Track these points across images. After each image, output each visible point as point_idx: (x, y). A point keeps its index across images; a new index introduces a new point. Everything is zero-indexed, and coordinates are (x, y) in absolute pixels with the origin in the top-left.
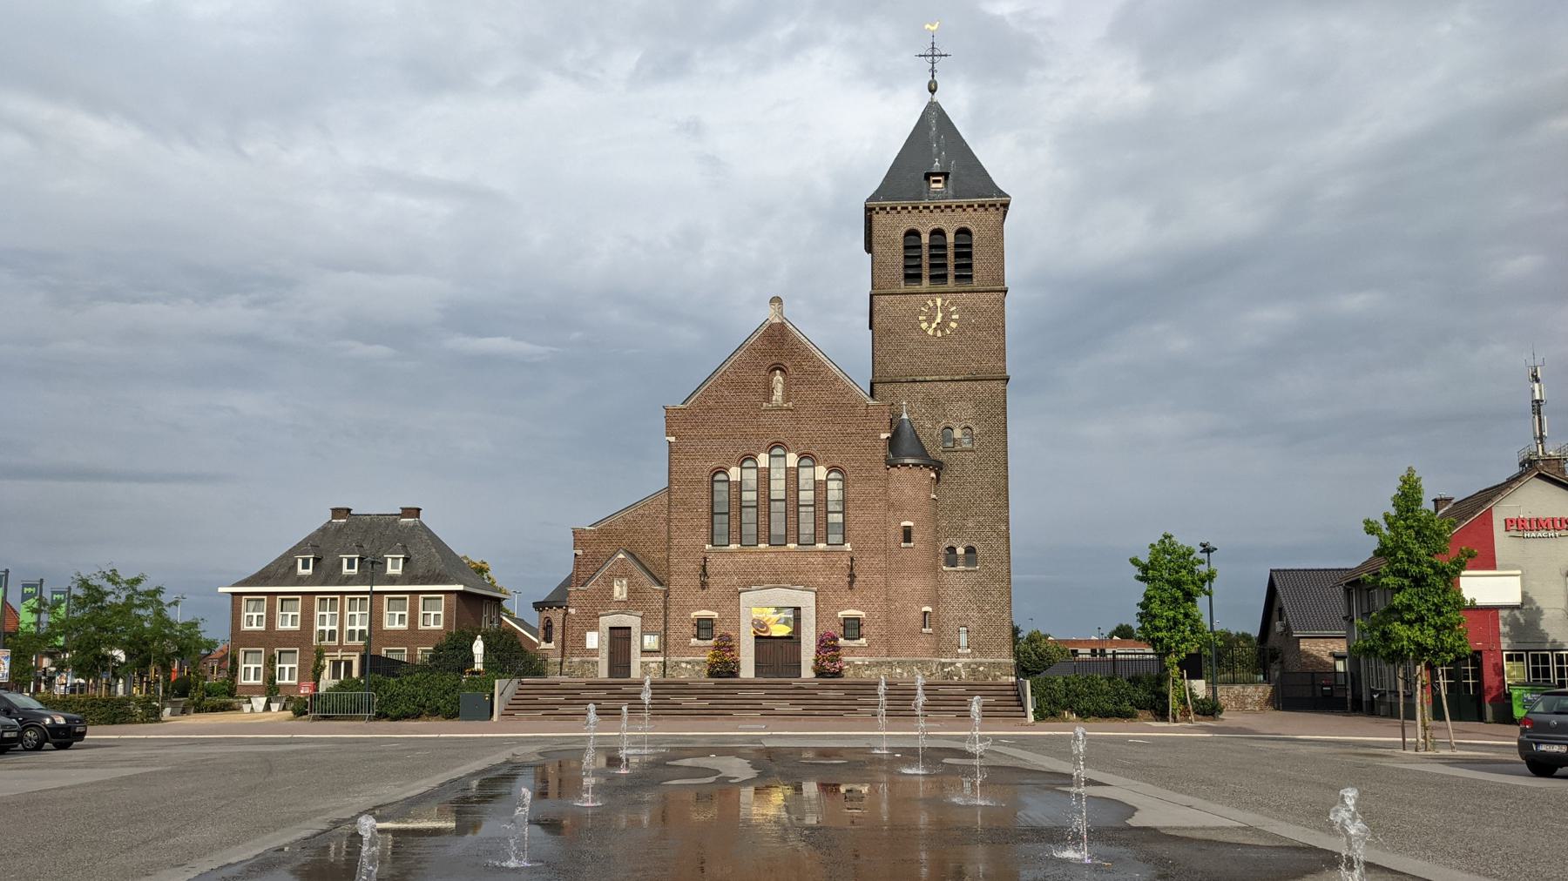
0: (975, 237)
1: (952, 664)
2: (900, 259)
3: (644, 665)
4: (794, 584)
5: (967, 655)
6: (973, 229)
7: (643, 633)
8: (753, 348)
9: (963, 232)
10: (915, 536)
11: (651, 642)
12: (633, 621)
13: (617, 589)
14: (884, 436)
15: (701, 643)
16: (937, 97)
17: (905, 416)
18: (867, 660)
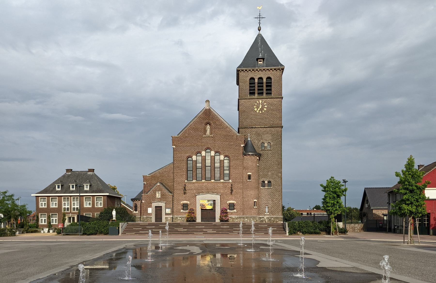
0: (273, 80)
1: (263, 218)
3: (166, 218)
5: (268, 215)
6: (272, 77)
7: (166, 208)
10: (252, 177)
12: (162, 204)
13: (157, 195)
14: (242, 145)
15: (184, 211)
16: (261, 32)
17: (249, 139)
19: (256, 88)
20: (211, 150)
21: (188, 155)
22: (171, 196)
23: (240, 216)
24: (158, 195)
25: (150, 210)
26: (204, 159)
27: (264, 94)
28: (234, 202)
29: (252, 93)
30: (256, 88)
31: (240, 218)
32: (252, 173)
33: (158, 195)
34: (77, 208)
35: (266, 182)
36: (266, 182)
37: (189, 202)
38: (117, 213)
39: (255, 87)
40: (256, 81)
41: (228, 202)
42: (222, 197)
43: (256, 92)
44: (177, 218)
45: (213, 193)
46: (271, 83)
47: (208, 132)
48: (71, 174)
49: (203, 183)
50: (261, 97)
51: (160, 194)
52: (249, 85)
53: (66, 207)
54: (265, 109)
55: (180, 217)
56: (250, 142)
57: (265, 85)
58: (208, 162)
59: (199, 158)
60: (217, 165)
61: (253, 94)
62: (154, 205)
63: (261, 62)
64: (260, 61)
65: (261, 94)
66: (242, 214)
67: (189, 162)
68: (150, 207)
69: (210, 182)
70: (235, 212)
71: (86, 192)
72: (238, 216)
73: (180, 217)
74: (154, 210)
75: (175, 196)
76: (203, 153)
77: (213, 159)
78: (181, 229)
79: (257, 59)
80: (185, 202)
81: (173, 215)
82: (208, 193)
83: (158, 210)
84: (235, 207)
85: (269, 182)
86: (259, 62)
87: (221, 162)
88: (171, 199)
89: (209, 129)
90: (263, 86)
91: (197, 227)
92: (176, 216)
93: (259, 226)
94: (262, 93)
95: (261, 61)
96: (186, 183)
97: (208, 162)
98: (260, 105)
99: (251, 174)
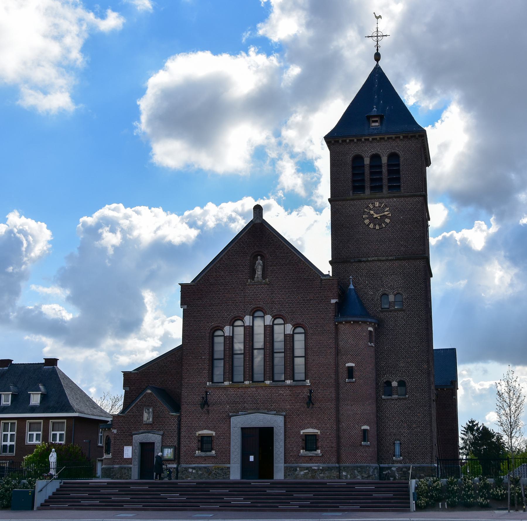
0: (402, 159)
1: (390, 468)
2: (350, 175)
5: (400, 462)
6: (401, 154)
7: (163, 447)
9: (393, 156)
10: (356, 374)
12: (155, 438)
13: (145, 415)
14: (333, 301)
15: (203, 454)
16: (380, 63)
17: (352, 287)
18: (322, 466)
19: (367, 177)
20: (265, 313)
21: (214, 324)
22: (176, 420)
23: (330, 465)
24: (147, 417)
25: (128, 452)
26: (249, 332)
27: (385, 190)
28: (316, 431)
29: (358, 187)
30: (367, 177)
31: (330, 469)
33: (147, 417)
34: (12, 446)
35: (394, 384)
36: (394, 384)
37: (214, 433)
38: (60, 461)
39: (363, 174)
40: (367, 161)
42: (288, 420)
43: (367, 184)
44: (186, 469)
45: (268, 410)
46: (398, 165)
47: (259, 273)
48: (8, 370)
49: (247, 387)
50: (378, 195)
51: (151, 415)
52: (350, 170)
53: (8, 443)
55: (193, 468)
56: (353, 293)
57: (385, 170)
58: (259, 340)
59: (240, 332)
60: (279, 345)
61: (362, 189)
62: (138, 438)
63: (377, 124)
64: (374, 122)
65: (377, 188)
66: (334, 459)
67: (216, 340)
68: (129, 443)
69: (262, 384)
70: (317, 456)
71: (33, 409)
72: (325, 465)
73: (193, 468)
74: (138, 451)
75: (184, 419)
76: (248, 320)
77: (269, 331)
78: (175, 496)
79: (369, 118)
80: (206, 432)
81: (179, 463)
82: (257, 410)
84: (319, 444)
85: (402, 384)
86: (373, 124)
87: (289, 339)
88: (175, 427)
89: (260, 267)
90: (381, 173)
92: (184, 466)
94: (380, 188)
95: (376, 121)
96: (209, 387)
97: (259, 340)
98: (378, 210)
99: (353, 365)
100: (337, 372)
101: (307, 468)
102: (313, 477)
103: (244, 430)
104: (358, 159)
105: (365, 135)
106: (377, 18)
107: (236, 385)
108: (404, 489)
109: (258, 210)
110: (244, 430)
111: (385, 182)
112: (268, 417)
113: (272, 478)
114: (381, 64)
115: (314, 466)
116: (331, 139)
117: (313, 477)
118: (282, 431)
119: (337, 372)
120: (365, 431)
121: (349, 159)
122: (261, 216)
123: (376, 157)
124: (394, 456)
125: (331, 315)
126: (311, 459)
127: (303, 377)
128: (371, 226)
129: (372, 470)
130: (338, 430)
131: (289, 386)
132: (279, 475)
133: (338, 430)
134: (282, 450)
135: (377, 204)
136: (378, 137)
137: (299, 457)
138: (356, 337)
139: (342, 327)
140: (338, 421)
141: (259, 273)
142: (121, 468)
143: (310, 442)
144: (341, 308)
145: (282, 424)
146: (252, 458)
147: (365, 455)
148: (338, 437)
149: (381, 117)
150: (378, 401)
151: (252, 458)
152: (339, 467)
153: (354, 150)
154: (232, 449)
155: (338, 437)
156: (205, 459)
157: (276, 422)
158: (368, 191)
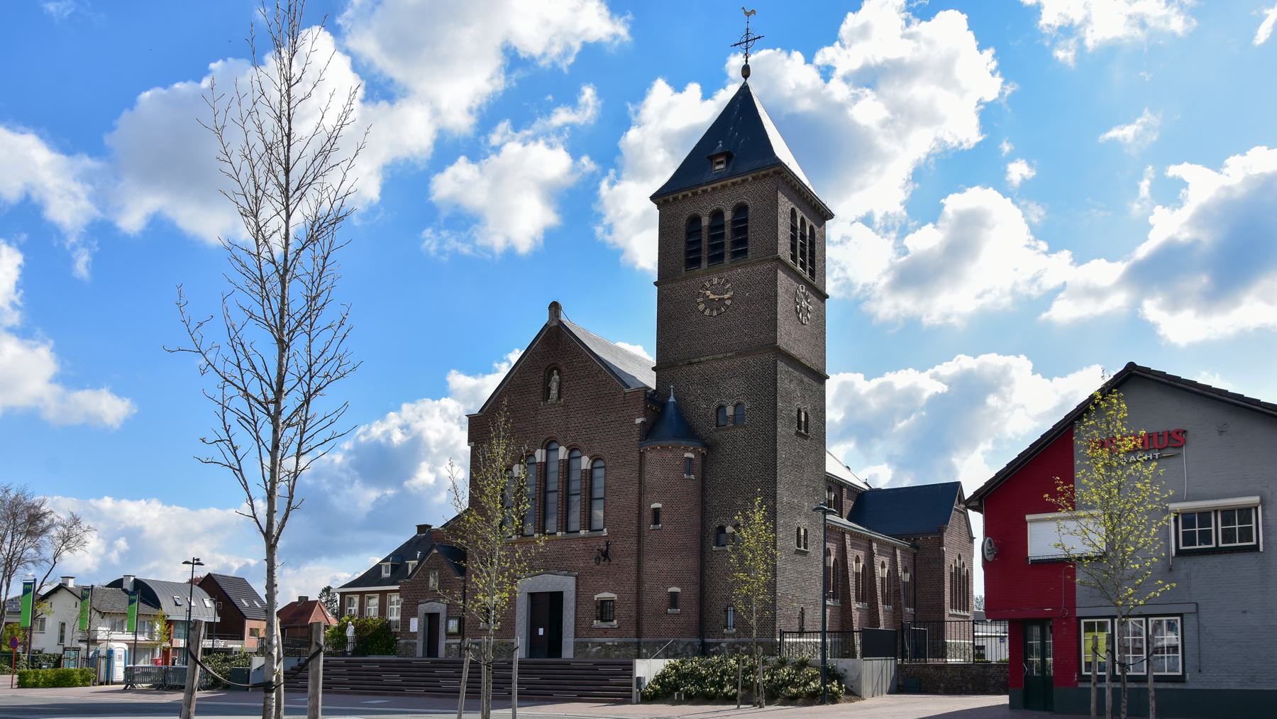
0: (750, 211)
1: (718, 644)
2: (682, 246)
3: (448, 646)
4: (560, 570)
5: (732, 636)
6: (750, 203)
7: (448, 618)
8: (91, 388)
9: (741, 209)
10: (663, 517)
11: (453, 625)
12: (439, 607)
13: (432, 580)
14: (638, 421)
15: (605, 625)
16: (749, 81)
17: (672, 399)
18: (617, 641)
24: (433, 582)
31: (626, 645)
32: (665, 503)
39: (700, 241)
41: (596, 597)
47: (554, 392)
54: (701, 307)
62: (424, 608)
63: (722, 166)
64: (718, 163)
66: (633, 633)
83: (432, 619)
91: (613, 681)
93: (601, 669)
100: (640, 515)
101: (600, 644)
102: (607, 656)
103: (532, 596)
104: (695, 220)
105: (701, 185)
106: (748, 14)
107: (525, 539)
108: (333, 679)
109: (555, 307)
110: (532, 596)
111: (728, 247)
112: (558, 578)
113: (560, 656)
114: (749, 81)
115: (608, 641)
116: (658, 197)
117: (607, 656)
118: (573, 596)
119: (640, 515)
120: (674, 595)
121: (683, 222)
122: (558, 316)
123: (717, 215)
124: (726, 627)
125: (636, 439)
126: (605, 632)
127: (601, 526)
128: (707, 312)
129: (681, 646)
130: (639, 593)
131: (583, 538)
132: (568, 653)
133: (639, 593)
134: (572, 620)
135: (715, 281)
136: (718, 185)
137: (591, 629)
138: (668, 465)
139: (648, 455)
140: (639, 582)
141: (554, 392)
142: (407, 644)
143: (604, 610)
144: (649, 432)
145: (573, 588)
146: (541, 632)
147: (672, 626)
148: (639, 603)
149: (729, 156)
150: (703, 553)
151: (541, 632)
152: (639, 643)
153: (688, 209)
154: (518, 620)
155: (639, 603)
156: (605, 632)
157: (565, 584)
158: (704, 264)
